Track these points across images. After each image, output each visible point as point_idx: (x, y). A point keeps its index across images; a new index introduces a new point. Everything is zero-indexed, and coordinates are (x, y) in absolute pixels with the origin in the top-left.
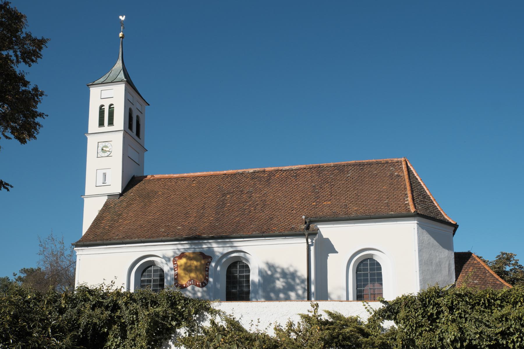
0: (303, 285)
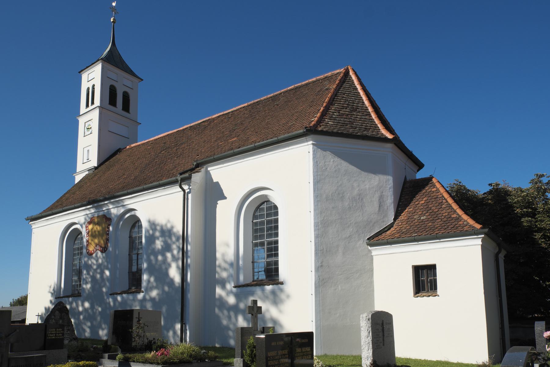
0: (177, 243)
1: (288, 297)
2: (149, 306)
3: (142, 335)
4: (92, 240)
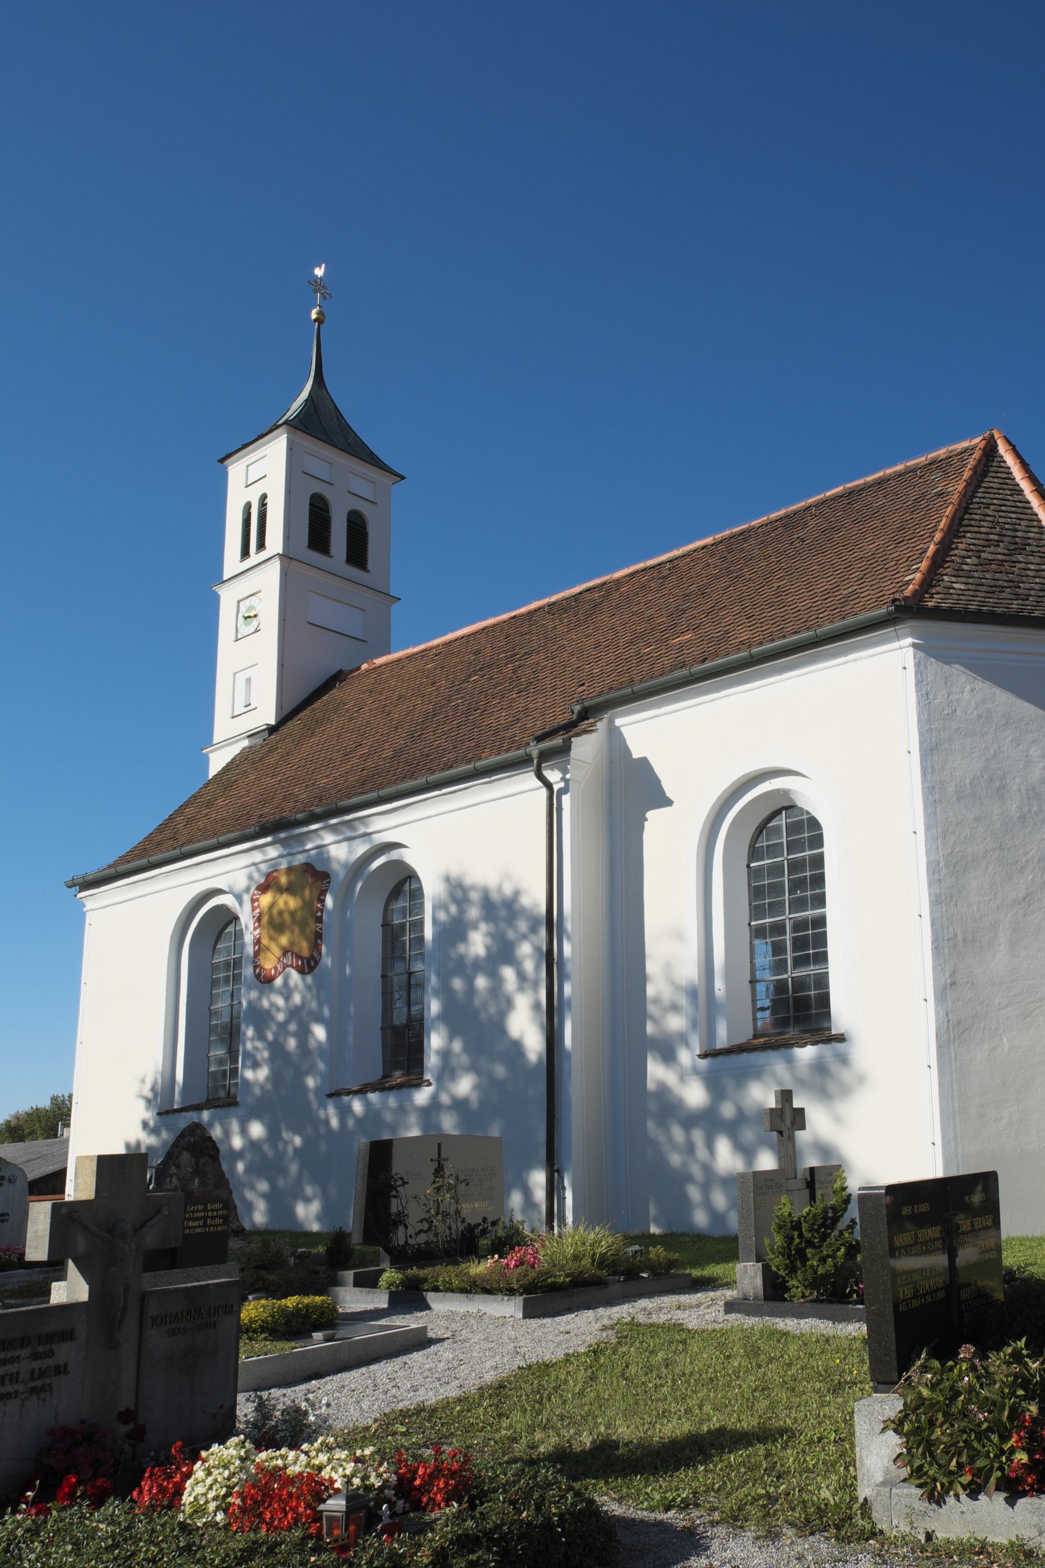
1: (862, 1079)
2: (449, 1124)
3: (452, 1212)
4: (271, 938)
